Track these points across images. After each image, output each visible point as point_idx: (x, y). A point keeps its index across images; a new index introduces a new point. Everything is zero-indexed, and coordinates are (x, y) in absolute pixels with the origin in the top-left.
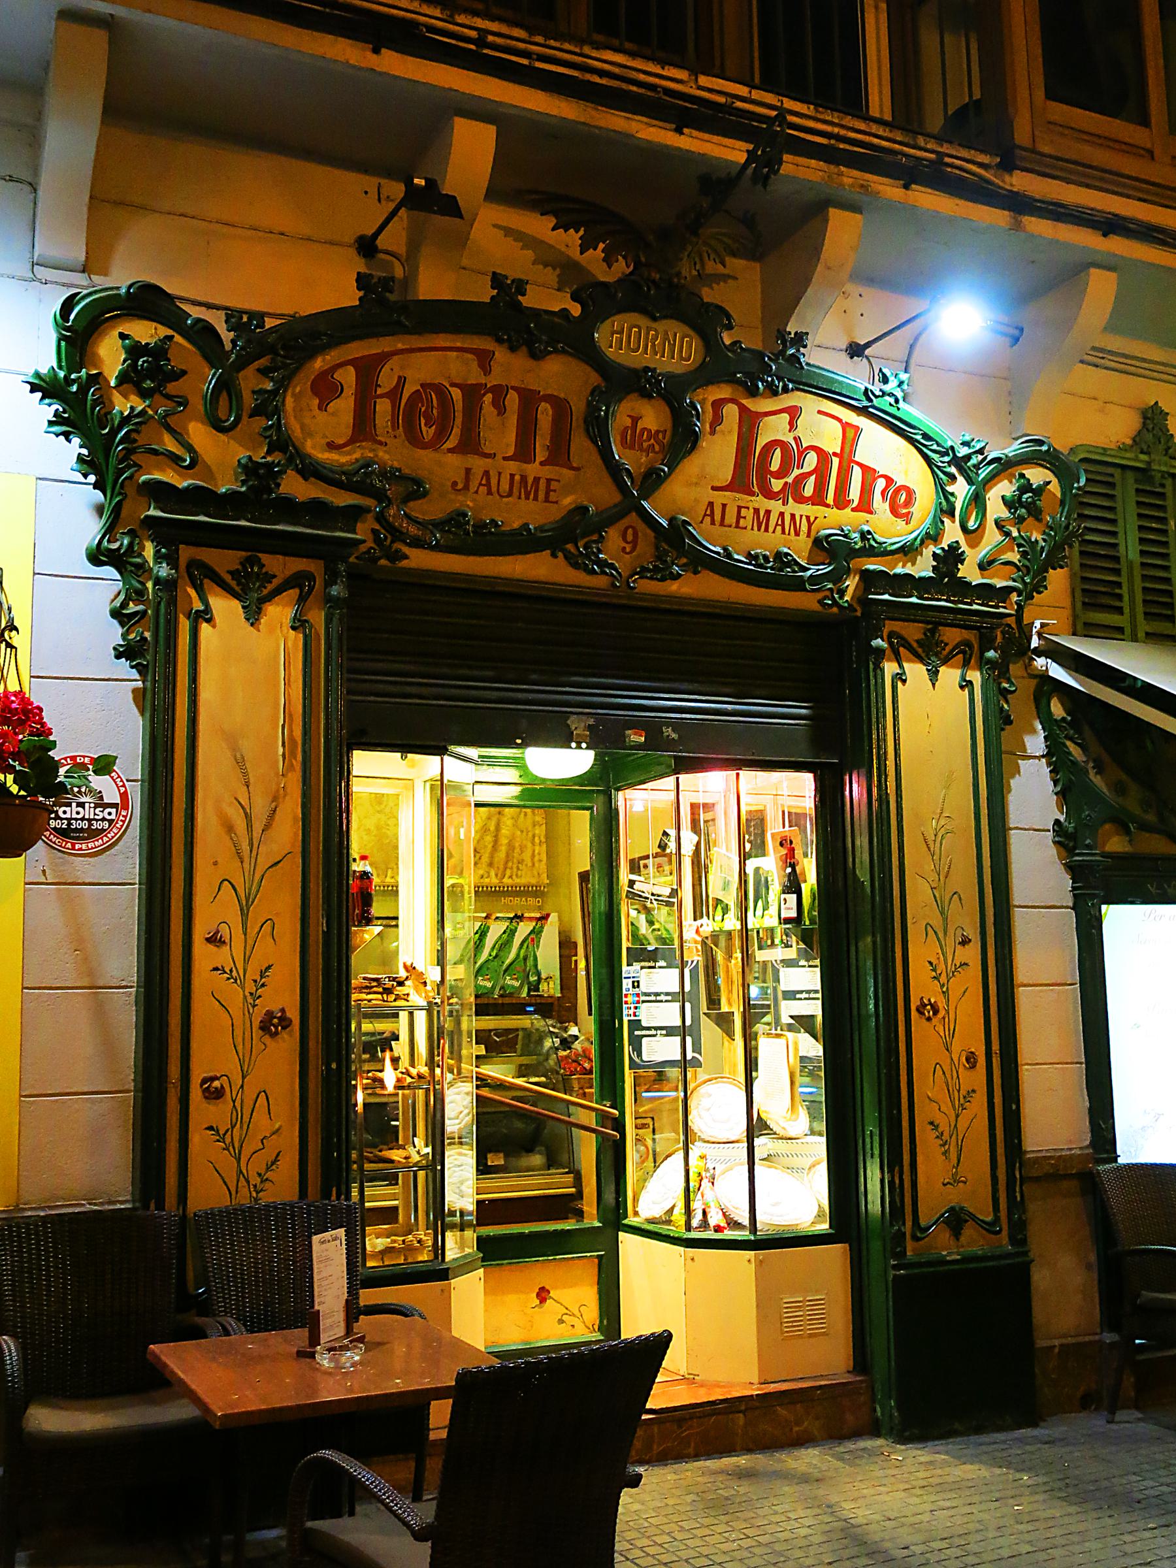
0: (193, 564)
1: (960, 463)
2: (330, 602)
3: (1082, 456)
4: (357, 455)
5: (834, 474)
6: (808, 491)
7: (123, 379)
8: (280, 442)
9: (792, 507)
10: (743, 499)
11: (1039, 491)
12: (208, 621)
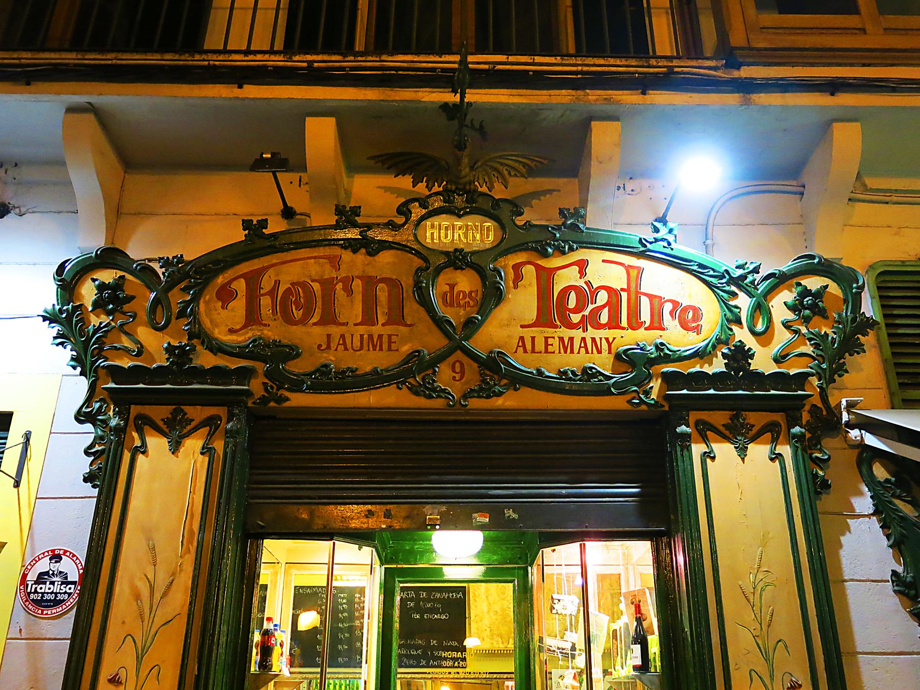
0: (139, 417)
1: (738, 281)
2: (229, 434)
3: (882, 270)
4: (250, 334)
5: (621, 307)
6: (604, 318)
7: (97, 305)
8: (198, 334)
9: (591, 332)
10: (549, 331)
11: (820, 294)
12: (143, 453)
